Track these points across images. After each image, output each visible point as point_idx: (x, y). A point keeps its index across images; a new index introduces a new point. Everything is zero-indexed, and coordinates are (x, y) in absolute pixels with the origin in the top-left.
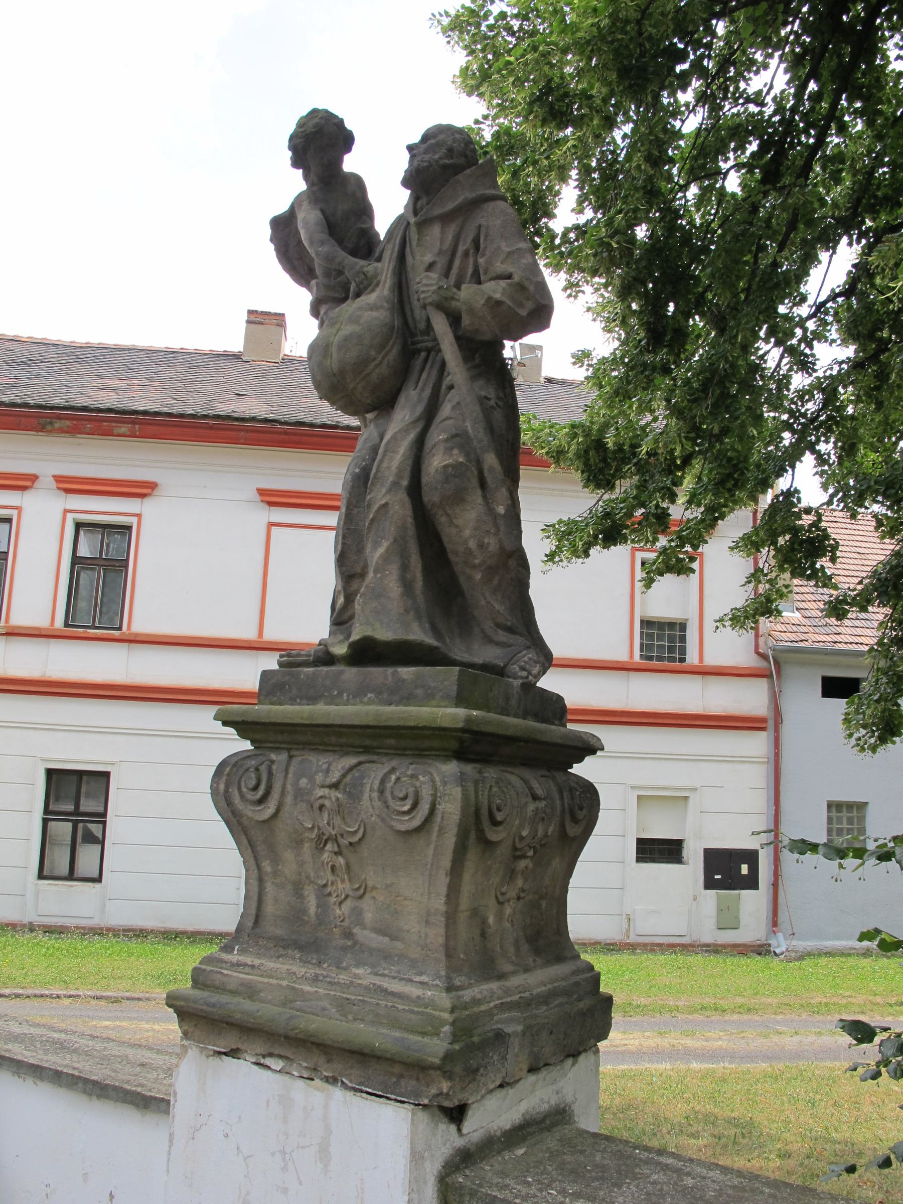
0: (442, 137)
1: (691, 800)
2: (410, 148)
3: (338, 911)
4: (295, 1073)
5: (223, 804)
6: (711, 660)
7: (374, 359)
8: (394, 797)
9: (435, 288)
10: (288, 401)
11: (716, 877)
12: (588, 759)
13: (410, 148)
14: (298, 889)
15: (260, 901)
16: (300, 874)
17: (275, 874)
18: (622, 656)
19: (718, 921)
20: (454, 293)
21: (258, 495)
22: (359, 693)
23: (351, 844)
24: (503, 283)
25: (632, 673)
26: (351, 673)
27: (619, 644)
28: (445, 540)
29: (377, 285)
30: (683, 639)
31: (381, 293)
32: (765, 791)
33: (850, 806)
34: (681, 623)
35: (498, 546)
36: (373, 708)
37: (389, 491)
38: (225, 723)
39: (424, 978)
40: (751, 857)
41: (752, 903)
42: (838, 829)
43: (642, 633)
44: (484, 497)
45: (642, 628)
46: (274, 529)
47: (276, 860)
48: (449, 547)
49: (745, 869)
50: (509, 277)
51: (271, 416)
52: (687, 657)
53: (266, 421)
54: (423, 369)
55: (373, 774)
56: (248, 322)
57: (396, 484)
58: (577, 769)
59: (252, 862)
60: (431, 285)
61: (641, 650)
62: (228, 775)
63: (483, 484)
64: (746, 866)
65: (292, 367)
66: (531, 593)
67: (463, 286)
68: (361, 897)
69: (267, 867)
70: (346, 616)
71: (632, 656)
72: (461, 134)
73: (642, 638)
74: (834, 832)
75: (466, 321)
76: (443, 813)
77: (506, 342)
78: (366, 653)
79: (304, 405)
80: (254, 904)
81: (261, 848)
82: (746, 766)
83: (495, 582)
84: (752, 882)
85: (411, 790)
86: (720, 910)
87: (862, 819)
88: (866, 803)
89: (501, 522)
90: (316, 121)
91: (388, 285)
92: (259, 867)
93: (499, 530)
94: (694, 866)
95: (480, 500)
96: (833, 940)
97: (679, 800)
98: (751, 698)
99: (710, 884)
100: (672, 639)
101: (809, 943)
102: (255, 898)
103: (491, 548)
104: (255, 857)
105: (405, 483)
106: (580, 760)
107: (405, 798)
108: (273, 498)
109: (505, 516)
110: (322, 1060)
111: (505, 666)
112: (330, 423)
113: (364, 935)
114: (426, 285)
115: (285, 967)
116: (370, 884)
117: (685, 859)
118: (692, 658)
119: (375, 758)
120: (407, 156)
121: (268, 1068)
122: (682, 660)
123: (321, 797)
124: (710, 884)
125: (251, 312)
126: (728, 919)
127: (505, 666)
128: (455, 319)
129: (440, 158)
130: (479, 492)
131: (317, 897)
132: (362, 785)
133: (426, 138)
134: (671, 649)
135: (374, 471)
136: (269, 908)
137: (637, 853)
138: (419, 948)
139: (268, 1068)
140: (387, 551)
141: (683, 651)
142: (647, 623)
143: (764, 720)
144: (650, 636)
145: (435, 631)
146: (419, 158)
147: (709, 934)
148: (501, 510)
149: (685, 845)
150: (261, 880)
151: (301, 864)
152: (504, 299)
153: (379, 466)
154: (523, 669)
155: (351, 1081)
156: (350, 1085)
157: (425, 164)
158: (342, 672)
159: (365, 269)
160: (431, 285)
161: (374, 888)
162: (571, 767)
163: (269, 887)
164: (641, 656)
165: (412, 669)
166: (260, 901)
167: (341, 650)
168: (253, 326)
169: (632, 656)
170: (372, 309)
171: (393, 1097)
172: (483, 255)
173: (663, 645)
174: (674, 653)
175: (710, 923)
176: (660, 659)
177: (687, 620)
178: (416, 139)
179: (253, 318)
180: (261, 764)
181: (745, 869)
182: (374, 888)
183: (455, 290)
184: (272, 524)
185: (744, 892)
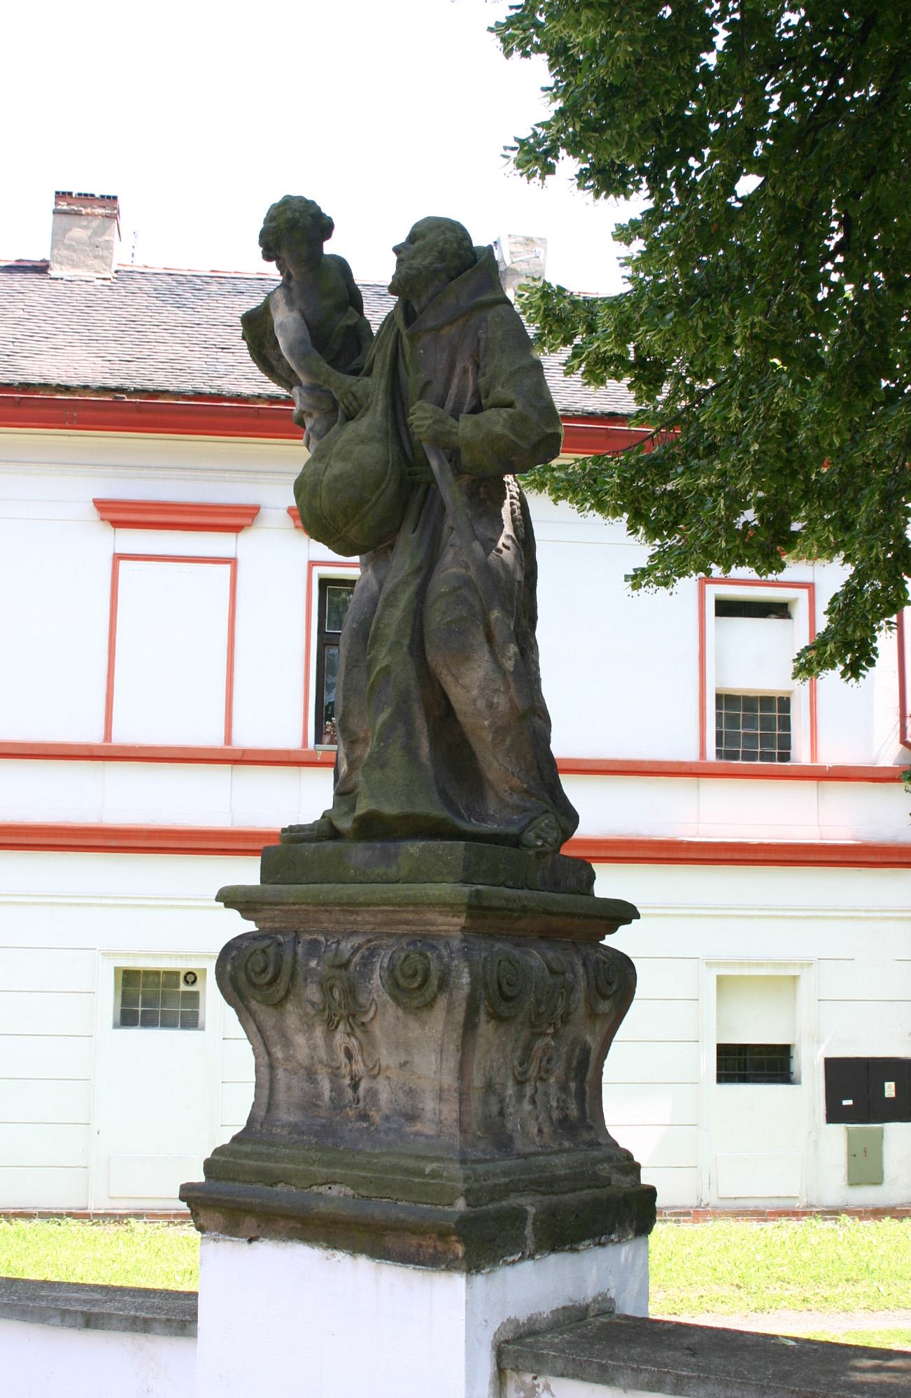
0: (430, 237)
1: (802, 984)
2: (397, 250)
5: (230, 989)
6: (829, 757)
7: (368, 501)
8: (403, 975)
9: (430, 421)
10: (136, 352)
11: (845, 1103)
12: (622, 929)
13: (397, 250)
14: (311, 1075)
15: (272, 1090)
16: (312, 1058)
17: (288, 1059)
18: (687, 753)
20: (453, 427)
21: (95, 510)
24: (504, 412)
25: (703, 780)
26: (359, 853)
27: (684, 733)
28: (452, 699)
29: (367, 409)
30: (786, 723)
31: (373, 419)
34: (781, 699)
35: (508, 705)
37: (390, 651)
38: (227, 905)
43: (718, 716)
44: (493, 653)
45: (718, 706)
46: (122, 564)
47: (287, 1043)
48: (456, 706)
50: (510, 405)
51: (113, 383)
52: (792, 752)
53: (105, 390)
54: (421, 508)
55: (383, 952)
56: (56, 212)
57: (397, 644)
58: (610, 941)
59: (262, 1049)
60: (426, 418)
61: (719, 743)
63: (489, 638)
64: (892, 1084)
65: (133, 287)
66: (538, 633)
67: (462, 416)
68: (375, 1077)
69: (278, 1053)
70: (350, 785)
71: (703, 753)
72: (454, 231)
73: (718, 724)
75: (465, 458)
77: (508, 478)
78: (372, 828)
79: (162, 357)
80: (266, 1092)
81: (272, 1034)
83: (508, 742)
85: (420, 967)
86: (852, 1155)
89: (510, 679)
90: (289, 214)
91: (380, 408)
92: (269, 1054)
93: (509, 687)
94: (811, 1084)
95: (487, 657)
97: (784, 984)
99: (835, 1114)
100: (767, 724)
102: (267, 1085)
103: (501, 708)
104: (265, 1045)
105: (406, 641)
106: (613, 930)
107: (414, 975)
108: (119, 514)
109: (513, 673)
111: (521, 833)
112: (208, 390)
114: (420, 419)
115: (282, 1165)
116: (383, 1063)
117: (793, 1077)
118: (801, 754)
120: (394, 258)
122: (785, 757)
124: (835, 1114)
125: (60, 195)
127: (521, 833)
128: (453, 456)
129: (431, 264)
130: (486, 648)
132: (373, 964)
133: (413, 237)
134: (767, 740)
135: (373, 628)
136: (281, 1097)
137: (718, 1069)
140: (391, 716)
141: (786, 742)
142: (725, 701)
144: (732, 721)
145: (449, 804)
146: (407, 265)
147: (835, 1189)
148: (509, 665)
149: (794, 1053)
150: (272, 1067)
151: (314, 1048)
152: (507, 432)
153: (378, 622)
154: (538, 837)
157: (414, 272)
159: (354, 389)
160: (426, 418)
161: (388, 1067)
162: (603, 938)
163: (280, 1074)
164: (718, 752)
165: (421, 844)
166: (272, 1090)
167: (345, 824)
168: (65, 218)
169: (703, 753)
170: (362, 442)
172: (484, 374)
173: (752, 733)
174: (772, 746)
176: (750, 756)
177: (790, 692)
178: (402, 238)
179: (64, 206)
183: (452, 421)
184: (118, 557)
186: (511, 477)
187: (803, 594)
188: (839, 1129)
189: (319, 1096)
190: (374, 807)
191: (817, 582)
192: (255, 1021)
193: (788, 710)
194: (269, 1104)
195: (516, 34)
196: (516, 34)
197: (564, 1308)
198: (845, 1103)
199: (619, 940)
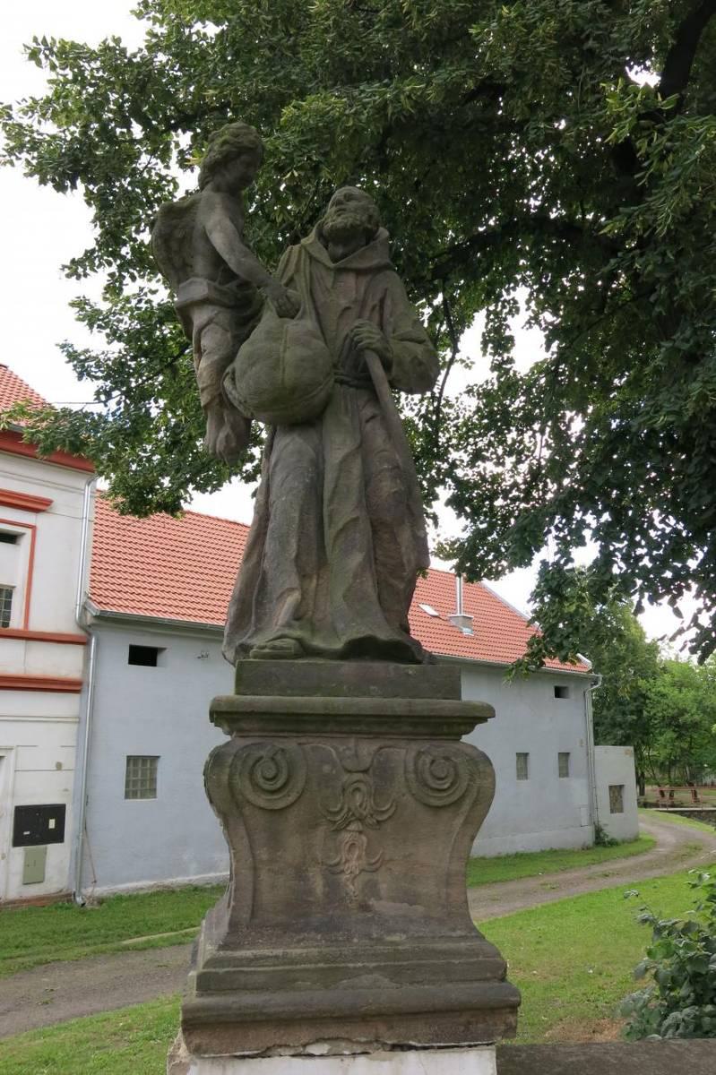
3: (351, 887)
4: (347, 1052)
6: (37, 625)
11: (26, 833)
12: (478, 727)
14: (300, 873)
19: (24, 876)
22: (359, 689)
23: (378, 822)
30: (8, 605)
32: (73, 750)
33: (144, 759)
36: (377, 700)
39: (459, 933)
40: (58, 811)
41: (57, 857)
42: (134, 781)
49: (52, 824)
62: (231, 766)
74: (131, 784)
76: (479, 789)
82: (60, 725)
84: (57, 836)
86: (27, 866)
87: (153, 771)
88: (158, 757)
96: (138, 880)
98: (64, 662)
99: (18, 841)
101: (105, 888)
104: (251, 848)
110: (382, 1029)
113: (382, 906)
118: (16, 622)
119: (390, 743)
121: (311, 1056)
123: (357, 781)
126: (34, 874)
131: (325, 877)
138: (439, 909)
139: (311, 1056)
143: (79, 683)
155: (419, 1042)
156: (419, 1045)
158: (342, 665)
163: (264, 876)
171: (466, 1043)
175: (16, 880)
177: (14, 587)
180: (275, 754)
181: (52, 824)
182: (391, 860)
185: (50, 846)
186: (531, 348)
187: (29, 532)
188: (20, 850)
189: (310, 892)
190: (369, 633)
191: (38, 525)
192: (245, 825)
193: (11, 597)
194: (253, 906)
195: (94, 132)
196: (94, 132)
197: (497, 1058)
198: (26, 833)
199: (477, 738)
